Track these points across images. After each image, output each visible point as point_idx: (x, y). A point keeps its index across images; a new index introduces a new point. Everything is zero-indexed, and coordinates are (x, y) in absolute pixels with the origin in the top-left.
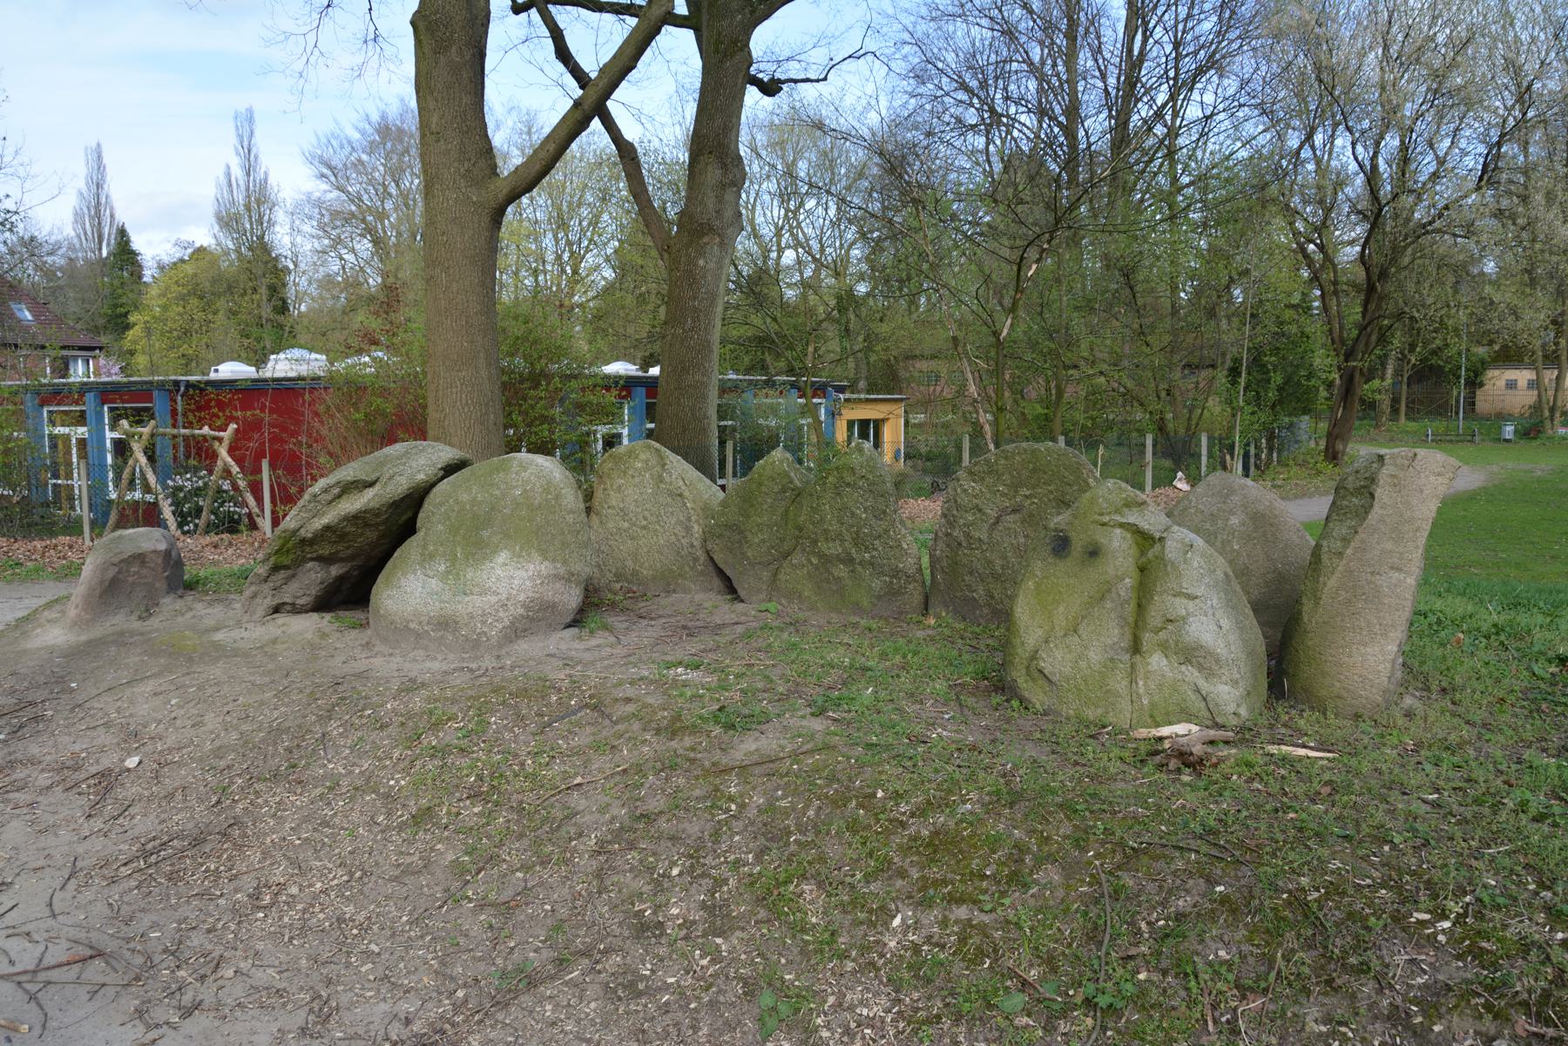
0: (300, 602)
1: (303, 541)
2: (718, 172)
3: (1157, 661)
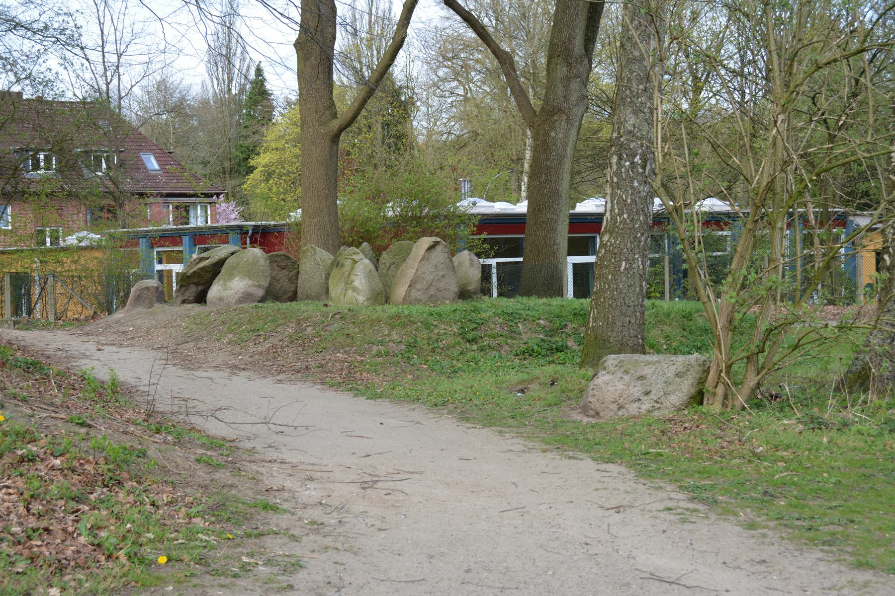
0: (190, 299)
1: (188, 276)
2: (565, 69)
3: (350, 292)
